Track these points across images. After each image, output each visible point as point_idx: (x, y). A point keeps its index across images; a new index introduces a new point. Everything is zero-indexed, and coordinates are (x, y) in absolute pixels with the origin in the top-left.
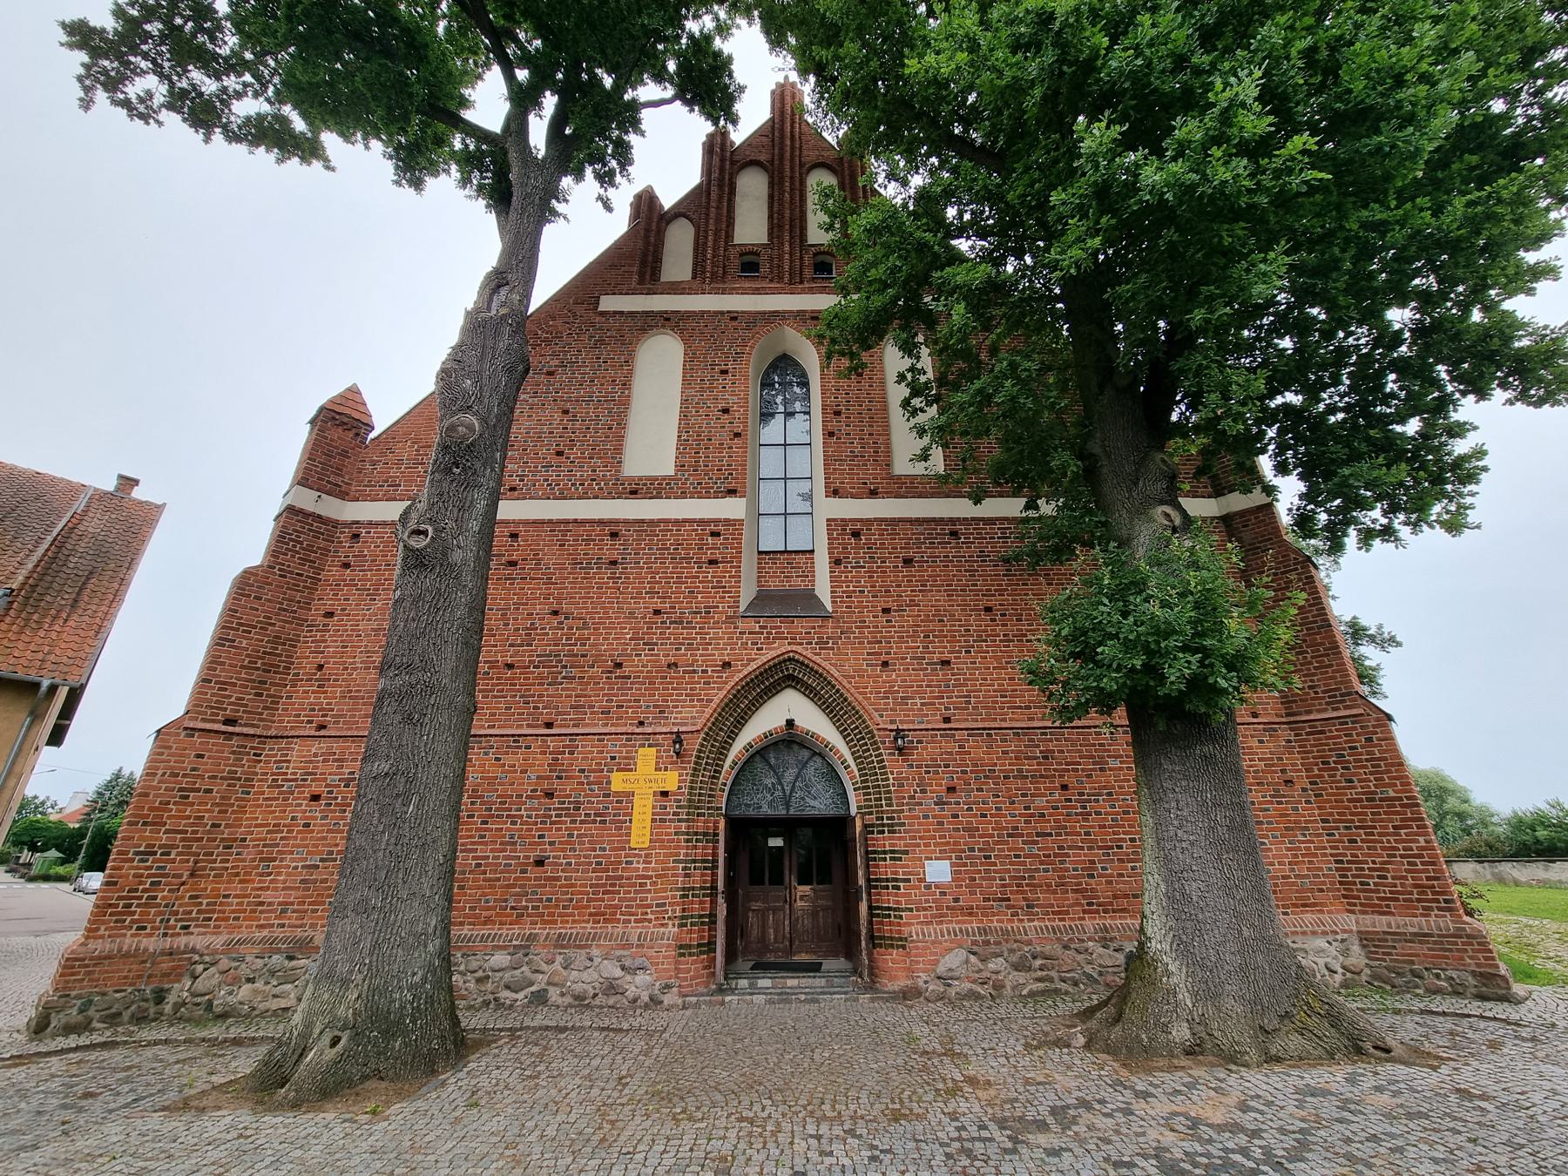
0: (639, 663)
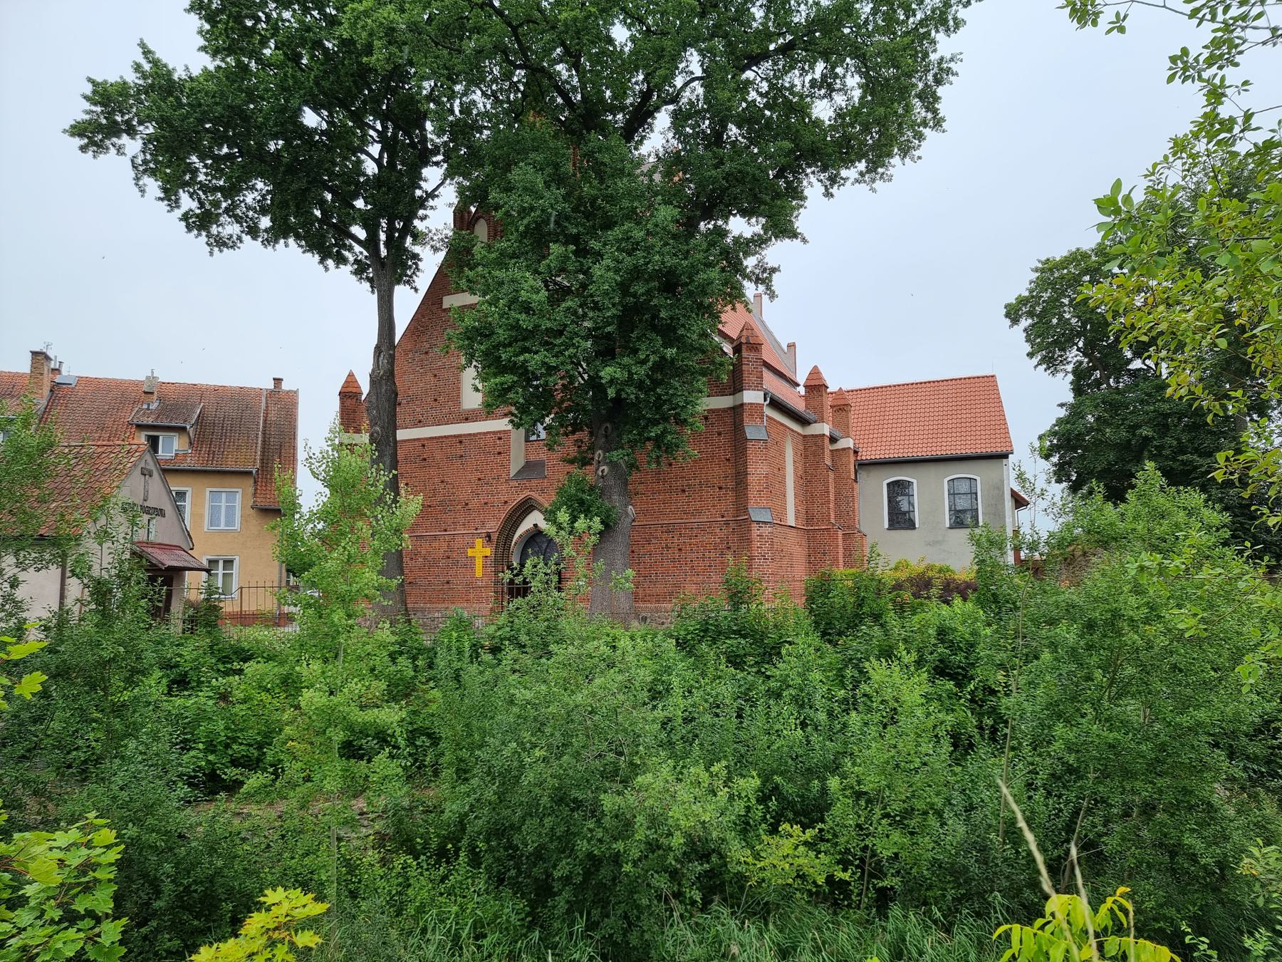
0: (474, 503)
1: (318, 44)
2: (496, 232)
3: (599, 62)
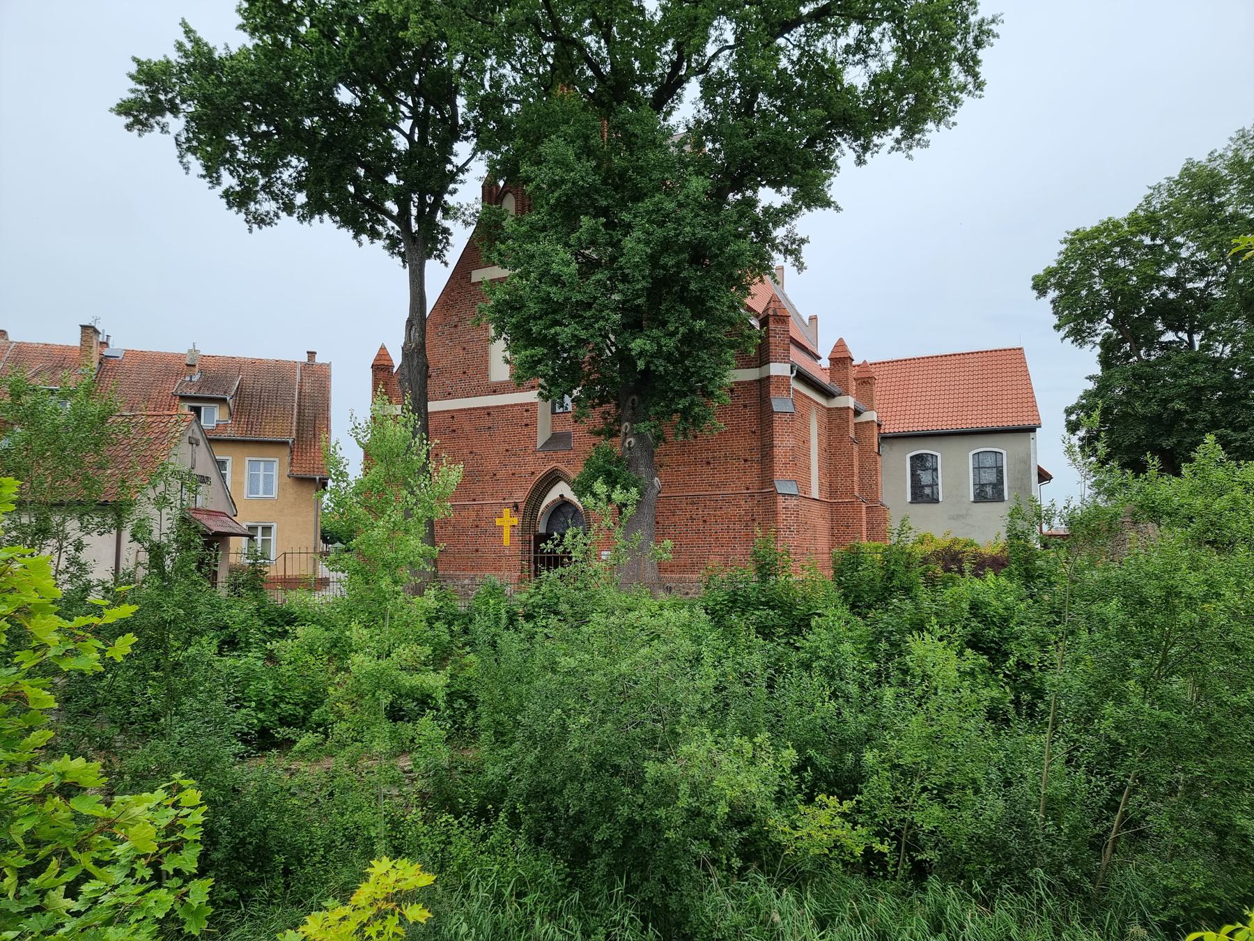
0: (502, 474)
1: (353, 20)
2: (525, 206)
3: (629, 33)
